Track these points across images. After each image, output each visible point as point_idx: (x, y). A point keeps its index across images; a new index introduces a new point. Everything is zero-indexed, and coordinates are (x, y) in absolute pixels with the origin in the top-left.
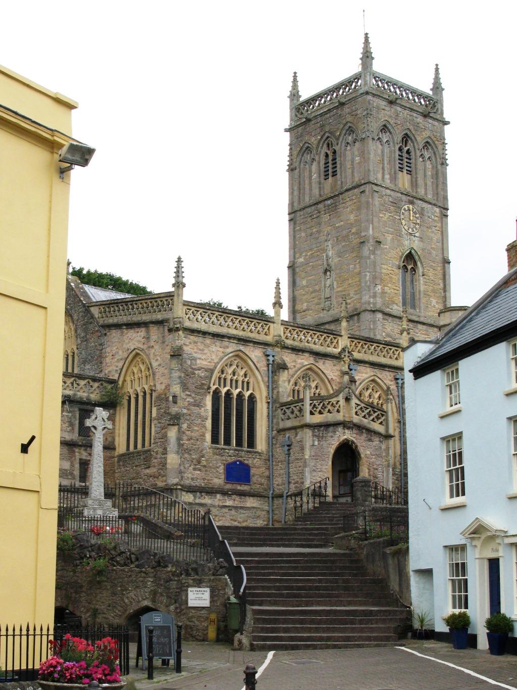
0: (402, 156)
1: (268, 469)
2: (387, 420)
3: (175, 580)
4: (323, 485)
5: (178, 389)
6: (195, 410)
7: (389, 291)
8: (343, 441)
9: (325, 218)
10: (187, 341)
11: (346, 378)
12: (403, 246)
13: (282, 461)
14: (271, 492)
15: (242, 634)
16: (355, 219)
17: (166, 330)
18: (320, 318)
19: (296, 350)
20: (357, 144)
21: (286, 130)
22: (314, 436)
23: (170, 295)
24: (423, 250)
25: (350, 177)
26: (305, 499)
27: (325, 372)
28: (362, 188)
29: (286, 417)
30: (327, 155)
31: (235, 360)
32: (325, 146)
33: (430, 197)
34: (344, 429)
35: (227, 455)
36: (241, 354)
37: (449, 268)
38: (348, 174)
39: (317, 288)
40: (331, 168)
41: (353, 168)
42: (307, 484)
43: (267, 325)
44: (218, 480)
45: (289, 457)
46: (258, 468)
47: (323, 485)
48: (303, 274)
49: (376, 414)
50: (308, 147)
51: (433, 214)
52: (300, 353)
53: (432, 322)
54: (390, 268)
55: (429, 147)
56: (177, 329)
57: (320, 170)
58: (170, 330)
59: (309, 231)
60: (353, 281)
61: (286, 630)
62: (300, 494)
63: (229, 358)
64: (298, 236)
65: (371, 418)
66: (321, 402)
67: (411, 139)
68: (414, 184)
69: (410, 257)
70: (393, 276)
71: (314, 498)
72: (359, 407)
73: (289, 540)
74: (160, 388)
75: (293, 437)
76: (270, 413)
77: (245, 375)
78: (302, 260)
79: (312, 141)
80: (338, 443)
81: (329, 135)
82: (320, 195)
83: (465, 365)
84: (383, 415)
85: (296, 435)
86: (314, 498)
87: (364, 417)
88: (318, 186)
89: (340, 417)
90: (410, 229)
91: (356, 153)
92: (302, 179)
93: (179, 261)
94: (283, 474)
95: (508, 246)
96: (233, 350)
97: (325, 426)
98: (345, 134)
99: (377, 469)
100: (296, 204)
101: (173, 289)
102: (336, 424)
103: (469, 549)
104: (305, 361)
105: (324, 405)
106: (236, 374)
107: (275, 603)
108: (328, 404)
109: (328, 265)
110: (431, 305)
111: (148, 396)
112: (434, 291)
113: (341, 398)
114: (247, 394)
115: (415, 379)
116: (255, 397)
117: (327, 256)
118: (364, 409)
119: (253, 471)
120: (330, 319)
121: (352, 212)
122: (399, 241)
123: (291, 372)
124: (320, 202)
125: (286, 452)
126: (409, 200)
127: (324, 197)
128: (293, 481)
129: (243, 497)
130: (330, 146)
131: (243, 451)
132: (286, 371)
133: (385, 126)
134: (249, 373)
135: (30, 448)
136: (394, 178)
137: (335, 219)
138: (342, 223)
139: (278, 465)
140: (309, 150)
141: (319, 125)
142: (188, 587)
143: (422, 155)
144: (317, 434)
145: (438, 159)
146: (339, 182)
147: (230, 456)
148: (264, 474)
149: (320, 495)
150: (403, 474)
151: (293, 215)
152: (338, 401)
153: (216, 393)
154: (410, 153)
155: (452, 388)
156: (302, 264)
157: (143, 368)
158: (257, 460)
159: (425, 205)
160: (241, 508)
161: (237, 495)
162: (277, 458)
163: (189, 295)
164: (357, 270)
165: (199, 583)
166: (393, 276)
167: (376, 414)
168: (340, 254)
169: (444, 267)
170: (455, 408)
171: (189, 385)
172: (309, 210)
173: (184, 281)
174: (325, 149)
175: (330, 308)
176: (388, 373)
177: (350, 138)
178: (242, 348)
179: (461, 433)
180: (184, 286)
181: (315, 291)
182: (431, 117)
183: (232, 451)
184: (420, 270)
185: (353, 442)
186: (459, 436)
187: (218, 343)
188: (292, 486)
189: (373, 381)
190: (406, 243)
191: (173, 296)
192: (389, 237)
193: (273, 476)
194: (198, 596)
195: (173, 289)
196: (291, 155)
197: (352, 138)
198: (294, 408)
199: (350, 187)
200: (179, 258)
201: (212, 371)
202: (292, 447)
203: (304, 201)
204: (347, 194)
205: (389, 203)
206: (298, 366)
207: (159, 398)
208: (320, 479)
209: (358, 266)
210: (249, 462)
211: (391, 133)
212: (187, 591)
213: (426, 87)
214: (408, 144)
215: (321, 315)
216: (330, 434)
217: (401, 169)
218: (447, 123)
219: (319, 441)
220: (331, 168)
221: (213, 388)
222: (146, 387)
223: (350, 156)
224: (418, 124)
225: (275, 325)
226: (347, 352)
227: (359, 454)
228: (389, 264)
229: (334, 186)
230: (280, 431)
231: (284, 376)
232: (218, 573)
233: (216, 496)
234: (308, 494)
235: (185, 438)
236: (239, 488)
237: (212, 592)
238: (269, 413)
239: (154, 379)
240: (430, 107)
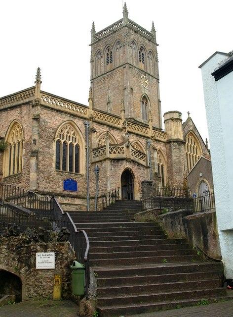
1: (87, 184)
2: (147, 159)
3: (25, 247)
4: (117, 191)
5: (37, 137)
6: (47, 150)
10: (43, 112)
15: (87, 299)
17: (31, 107)
19: (99, 123)
21: (89, 45)
22: (111, 164)
23: (33, 88)
26: (108, 198)
30: (108, 55)
32: (107, 50)
33: (152, 74)
40: (110, 60)
42: (109, 190)
44: (60, 189)
47: (117, 191)
56: (37, 105)
58: (33, 106)
59: (100, 87)
61: (128, 291)
62: (61, 239)
68: (146, 67)
73: (105, 218)
74: (27, 138)
85: (102, 165)
89: (124, 156)
93: (39, 69)
101: (35, 85)
102: (122, 159)
104: (105, 129)
107: (116, 263)
111: (21, 145)
113: (124, 146)
114: (75, 144)
115: (216, 81)
119: (78, 185)
134: (76, 133)
136: (137, 64)
146: (113, 65)
149: (116, 197)
153: (58, 142)
157: (18, 130)
160: (73, 204)
163: (44, 87)
165: (45, 249)
171: (43, 136)
173: (41, 80)
178: (72, 119)
180: (41, 82)
185: (131, 169)
187: (59, 115)
189: (137, 143)
191: (35, 88)
192: (136, 88)
194: (44, 259)
195: (35, 85)
196: (92, 55)
200: (39, 69)
201: (57, 129)
207: (27, 144)
210: (77, 180)
212: (35, 255)
213: (149, 30)
218: (158, 45)
220: (110, 60)
221: (57, 139)
222: (20, 140)
223: (119, 57)
228: (137, 99)
231: (94, 135)
235: (40, 164)
237: (56, 255)
239: (24, 134)
240: (151, 37)
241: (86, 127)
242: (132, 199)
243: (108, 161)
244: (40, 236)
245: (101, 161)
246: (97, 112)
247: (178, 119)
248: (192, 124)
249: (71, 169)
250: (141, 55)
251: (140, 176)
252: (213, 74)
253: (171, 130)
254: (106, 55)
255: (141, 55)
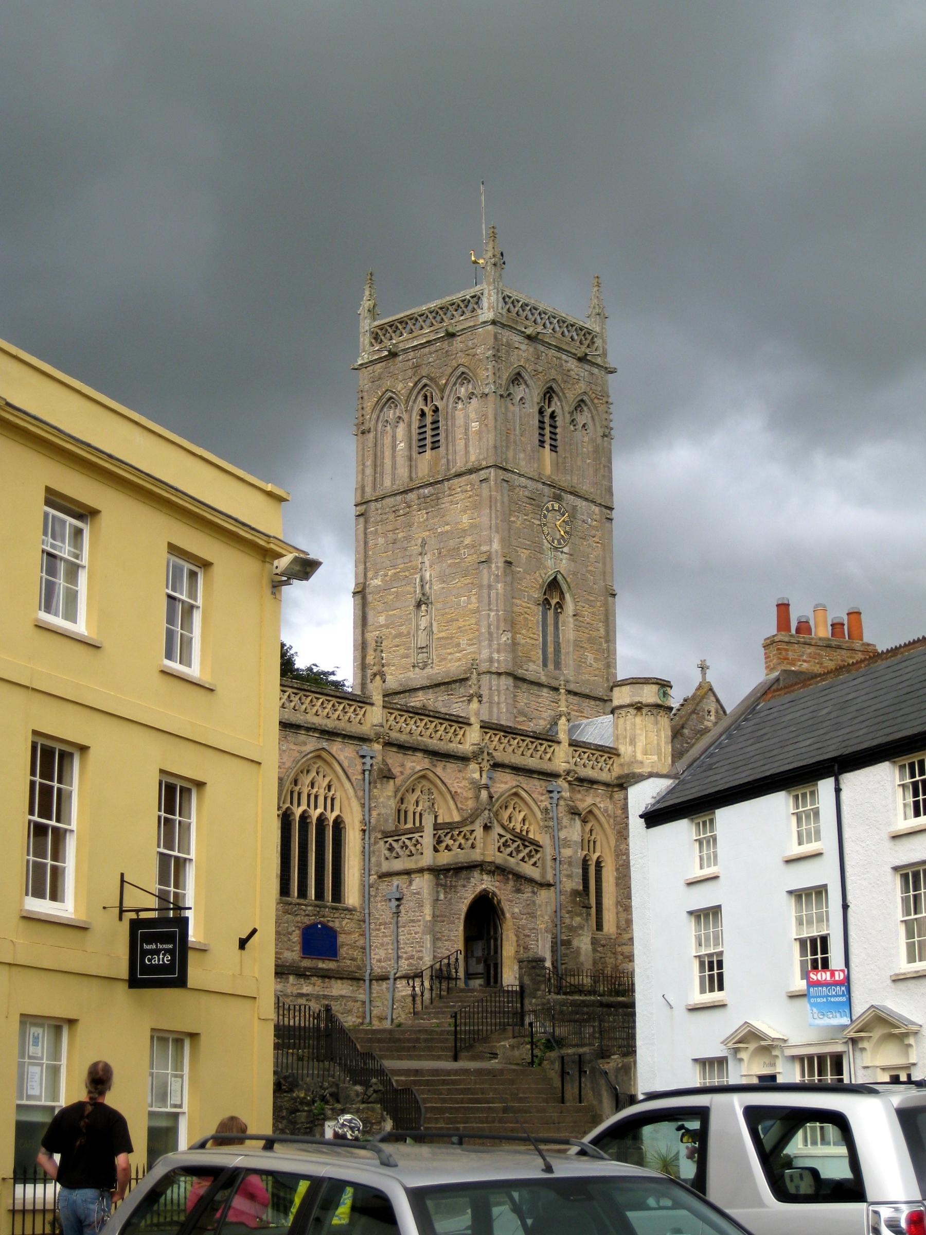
0: (555, 434)
3: (304, 1111)
4: (453, 960)
7: (523, 641)
8: (480, 892)
9: (420, 516)
11: (484, 794)
12: (545, 568)
13: (385, 924)
14: (368, 971)
16: (471, 524)
18: (409, 679)
20: (474, 401)
24: (575, 574)
25: (463, 452)
27: (446, 780)
28: (483, 474)
29: (394, 854)
30: (423, 414)
31: (314, 763)
32: (420, 398)
34: (481, 874)
35: (303, 913)
36: (324, 754)
37: (614, 603)
38: (458, 448)
39: (404, 629)
41: (467, 440)
43: (361, 708)
45: (398, 917)
46: (350, 934)
48: (380, 607)
49: (528, 850)
50: (391, 398)
51: (589, 516)
52: (410, 753)
53: (587, 691)
54: (524, 604)
55: (585, 409)
57: (410, 439)
60: (467, 623)
63: (307, 760)
64: (371, 543)
65: (521, 855)
66: (448, 833)
67: (558, 396)
69: (554, 585)
70: (529, 617)
71: (440, 983)
72: (503, 840)
75: (405, 886)
76: (367, 846)
77: (329, 787)
78: (377, 582)
79: (399, 389)
80: (473, 896)
81: (428, 382)
82: (411, 479)
83: (725, 816)
84: (537, 851)
85: (411, 883)
86: (440, 983)
87: (510, 855)
88: (407, 463)
89: (476, 856)
90: (556, 542)
91: (473, 415)
92: (379, 448)
94: (388, 944)
95: (765, 640)
96: (313, 749)
97: (453, 869)
98: (455, 384)
99: (529, 936)
100: (368, 489)
102: (471, 867)
103: (731, 1063)
105: (452, 836)
106: (316, 785)
108: (458, 835)
109: (423, 594)
110: (585, 662)
112: (591, 640)
116: (343, 821)
117: (422, 580)
118: (510, 842)
119: (341, 939)
120: (427, 683)
121: (465, 511)
122: (539, 560)
123: (398, 781)
124: (411, 490)
125: (394, 910)
126: (554, 493)
127: (417, 483)
128: (405, 956)
129: (327, 980)
130: (429, 399)
131: (325, 907)
132: (392, 782)
133: (519, 374)
135: (248, 945)
137: (436, 520)
138: (448, 528)
139: (379, 930)
140: (393, 403)
141: (410, 363)
142: (325, 1119)
143: (573, 421)
144: (443, 882)
145: (599, 429)
146: (444, 461)
147: (308, 915)
148: (358, 944)
150: (559, 942)
151: (364, 506)
152: (473, 831)
154: (555, 417)
155: (708, 842)
156: (378, 590)
158: (346, 920)
159: (580, 503)
161: (318, 976)
162: (378, 919)
164: (474, 606)
166: (529, 617)
167: (528, 850)
168: (443, 578)
169: (605, 605)
170: (708, 871)
172: (390, 501)
174: (420, 404)
175: (426, 665)
176: (536, 782)
177: (463, 390)
178: (325, 744)
179: (719, 907)
181: (399, 635)
182: (589, 361)
183: (310, 908)
184: (570, 606)
185: (494, 894)
186: (716, 911)
188: (404, 964)
189: (516, 794)
190: (550, 563)
193: (370, 946)
197: (467, 390)
198: (406, 841)
199: (463, 469)
202: (404, 901)
203: (382, 485)
204: (456, 481)
205: (525, 500)
206: (408, 772)
208: (447, 953)
209: (474, 599)
210: (336, 925)
211: (527, 386)
212: (323, 1125)
214: (553, 404)
215: (411, 674)
216: (461, 882)
217: (542, 443)
219: (446, 892)
224: (568, 371)
225: (374, 708)
226: (486, 753)
227: (503, 914)
229: (434, 463)
230: (382, 876)
232: (371, 1099)
233: (288, 978)
234: (432, 976)
236: (321, 965)
238: (364, 848)
241: (364, 764)
242: (496, 981)
243: (427, 876)
244: (331, 1095)
245: (408, 873)
246: (397, 713)
247: (658, 706)
248: (713, 707)
249: (320, 895)
250: (547, 420)
251: (528, 930)
252: (641, 816)
253: (633, 742)
254: (416, 416)
255: (547, 420)
